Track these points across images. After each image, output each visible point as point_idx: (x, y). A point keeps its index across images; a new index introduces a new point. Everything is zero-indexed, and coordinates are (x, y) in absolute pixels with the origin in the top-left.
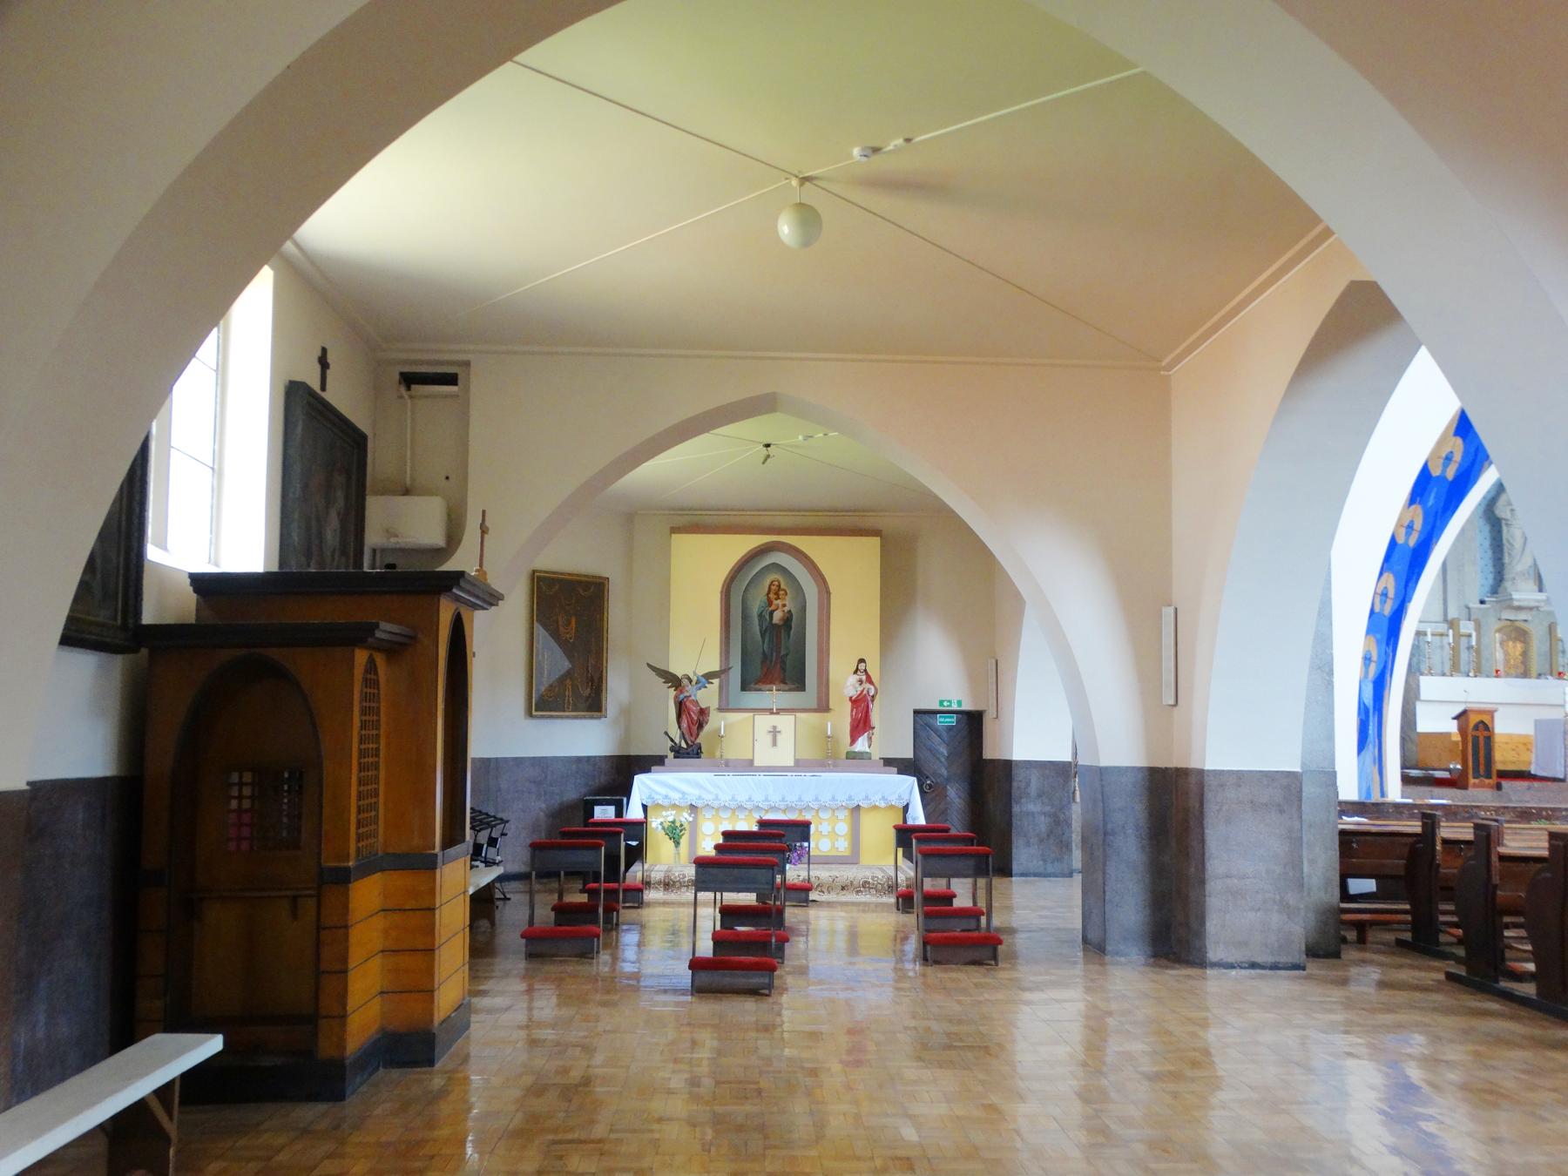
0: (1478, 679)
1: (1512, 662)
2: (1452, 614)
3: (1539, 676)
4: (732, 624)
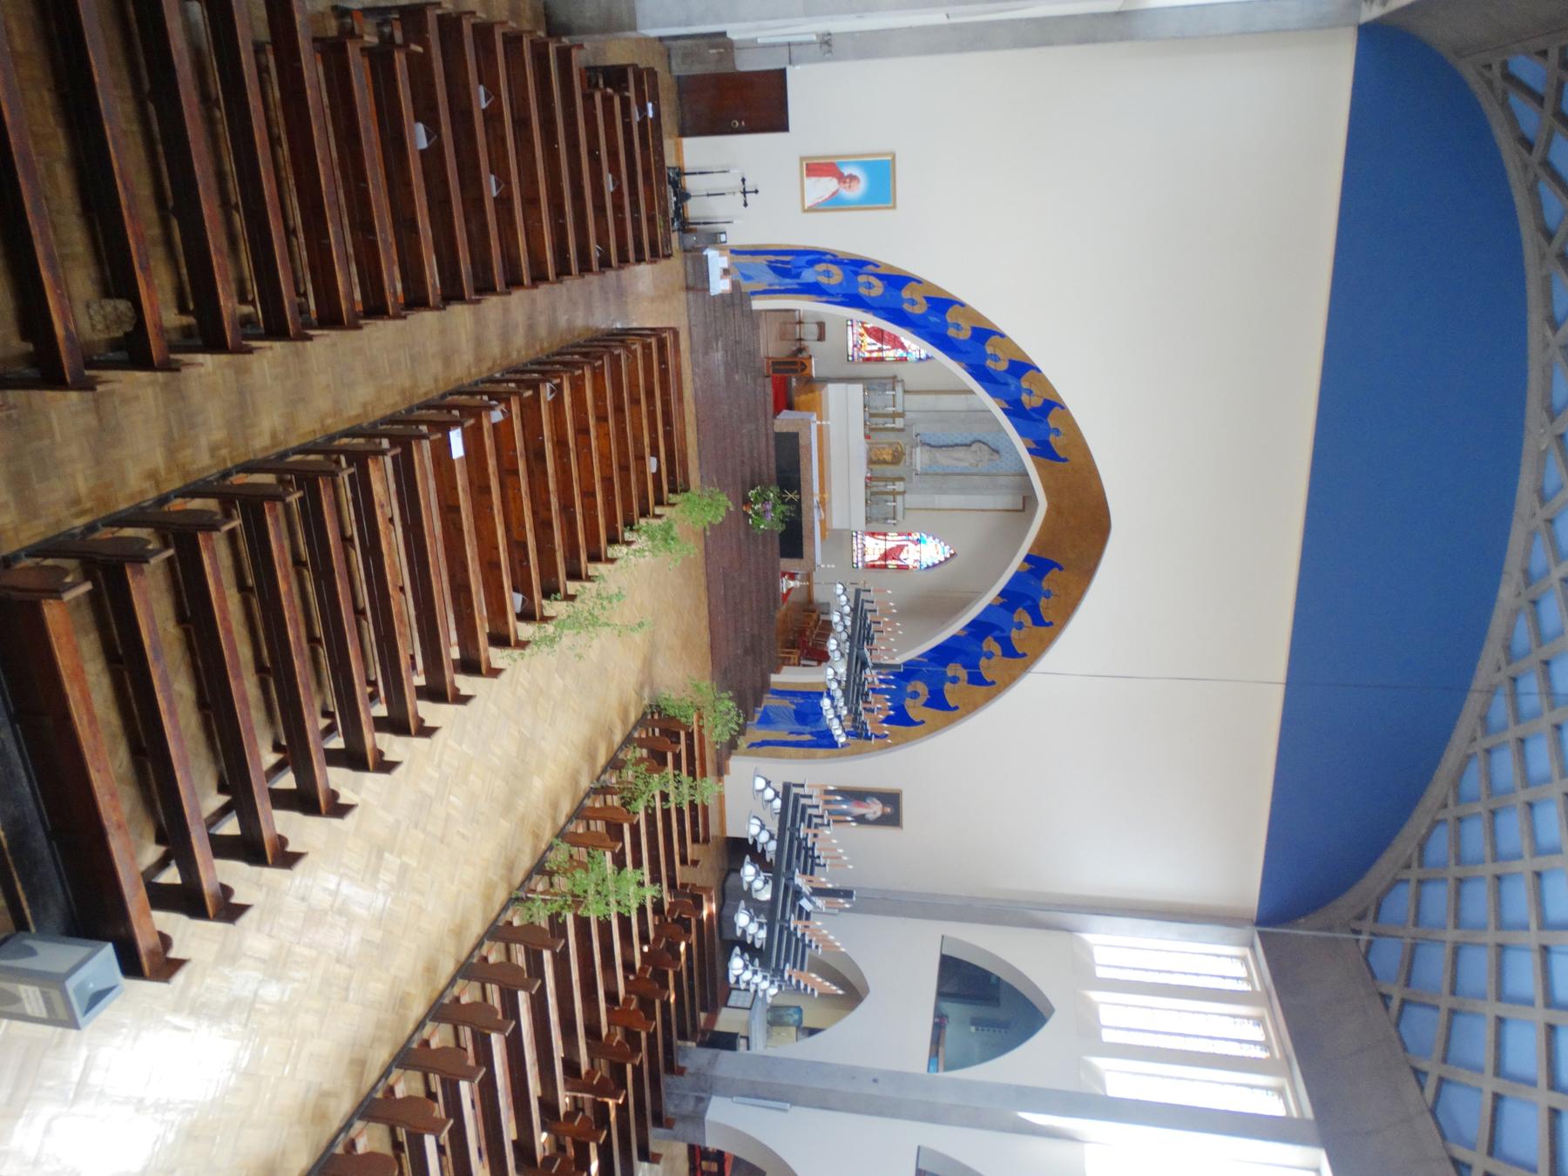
2: (909, 416)
4: (212, 181)
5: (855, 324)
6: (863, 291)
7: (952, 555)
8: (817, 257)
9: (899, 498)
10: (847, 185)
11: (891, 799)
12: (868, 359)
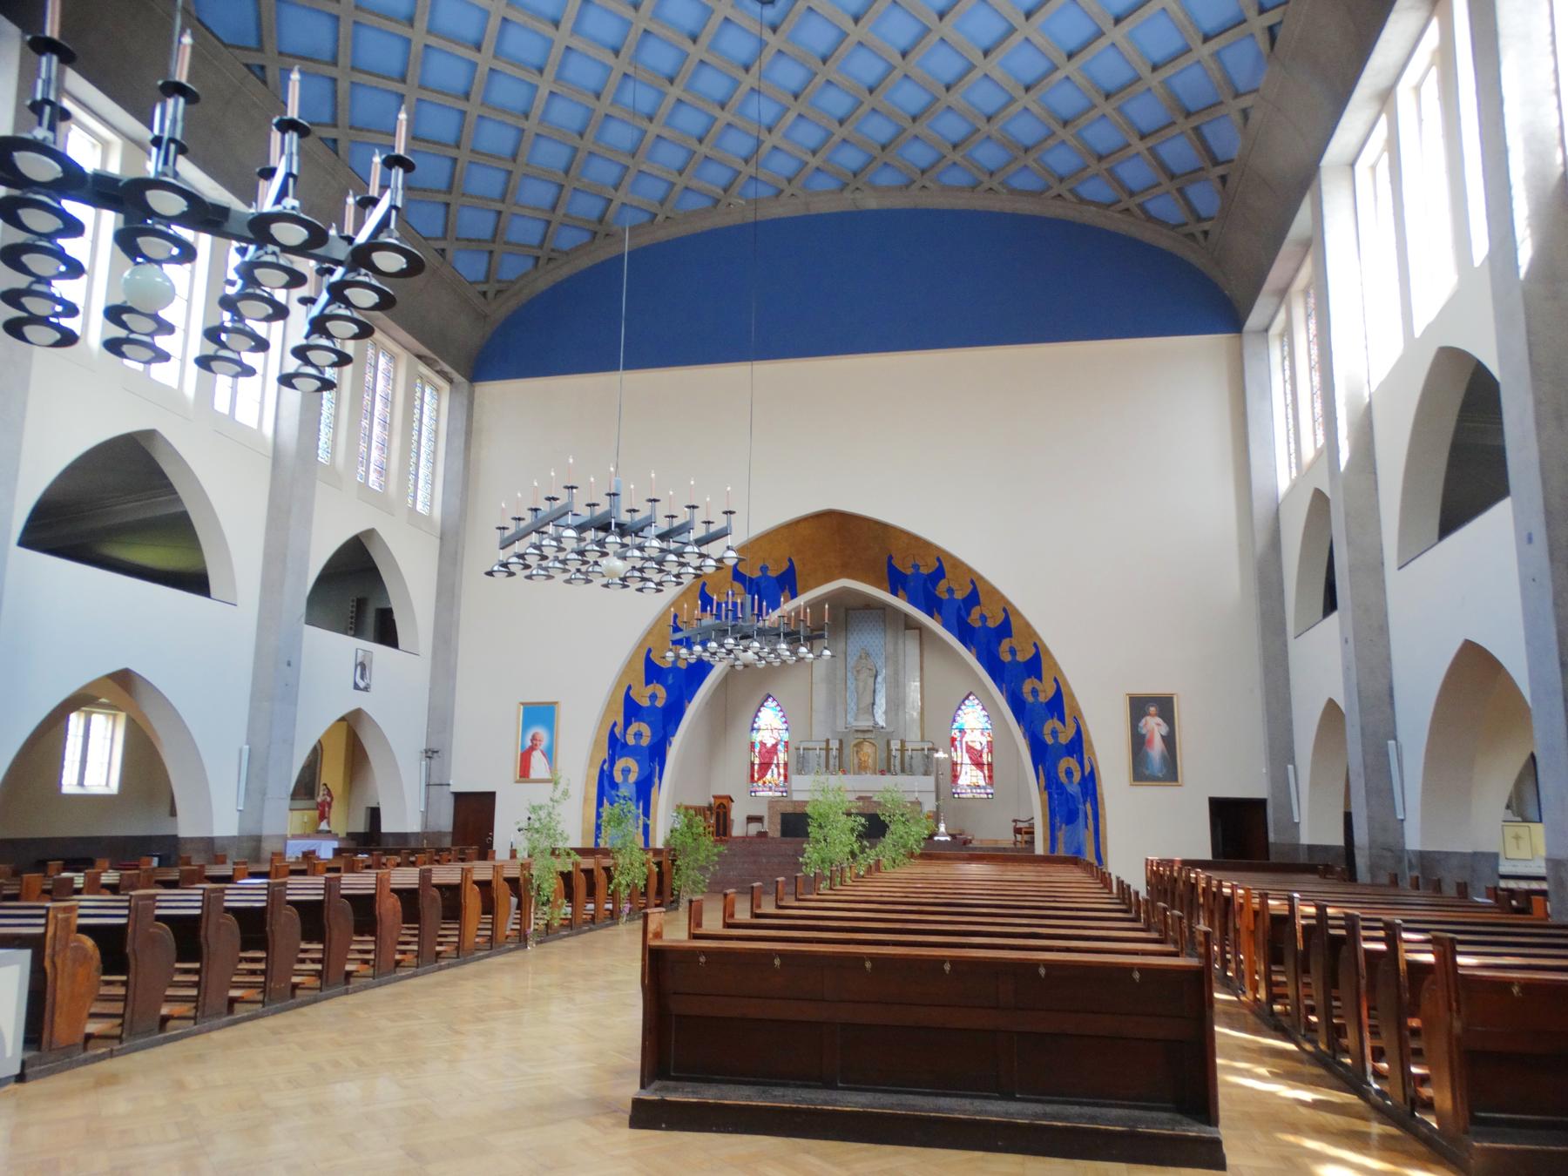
5: (753, 789)
8: (606, 783)
10: (538, 743)
11: (1139, 706)
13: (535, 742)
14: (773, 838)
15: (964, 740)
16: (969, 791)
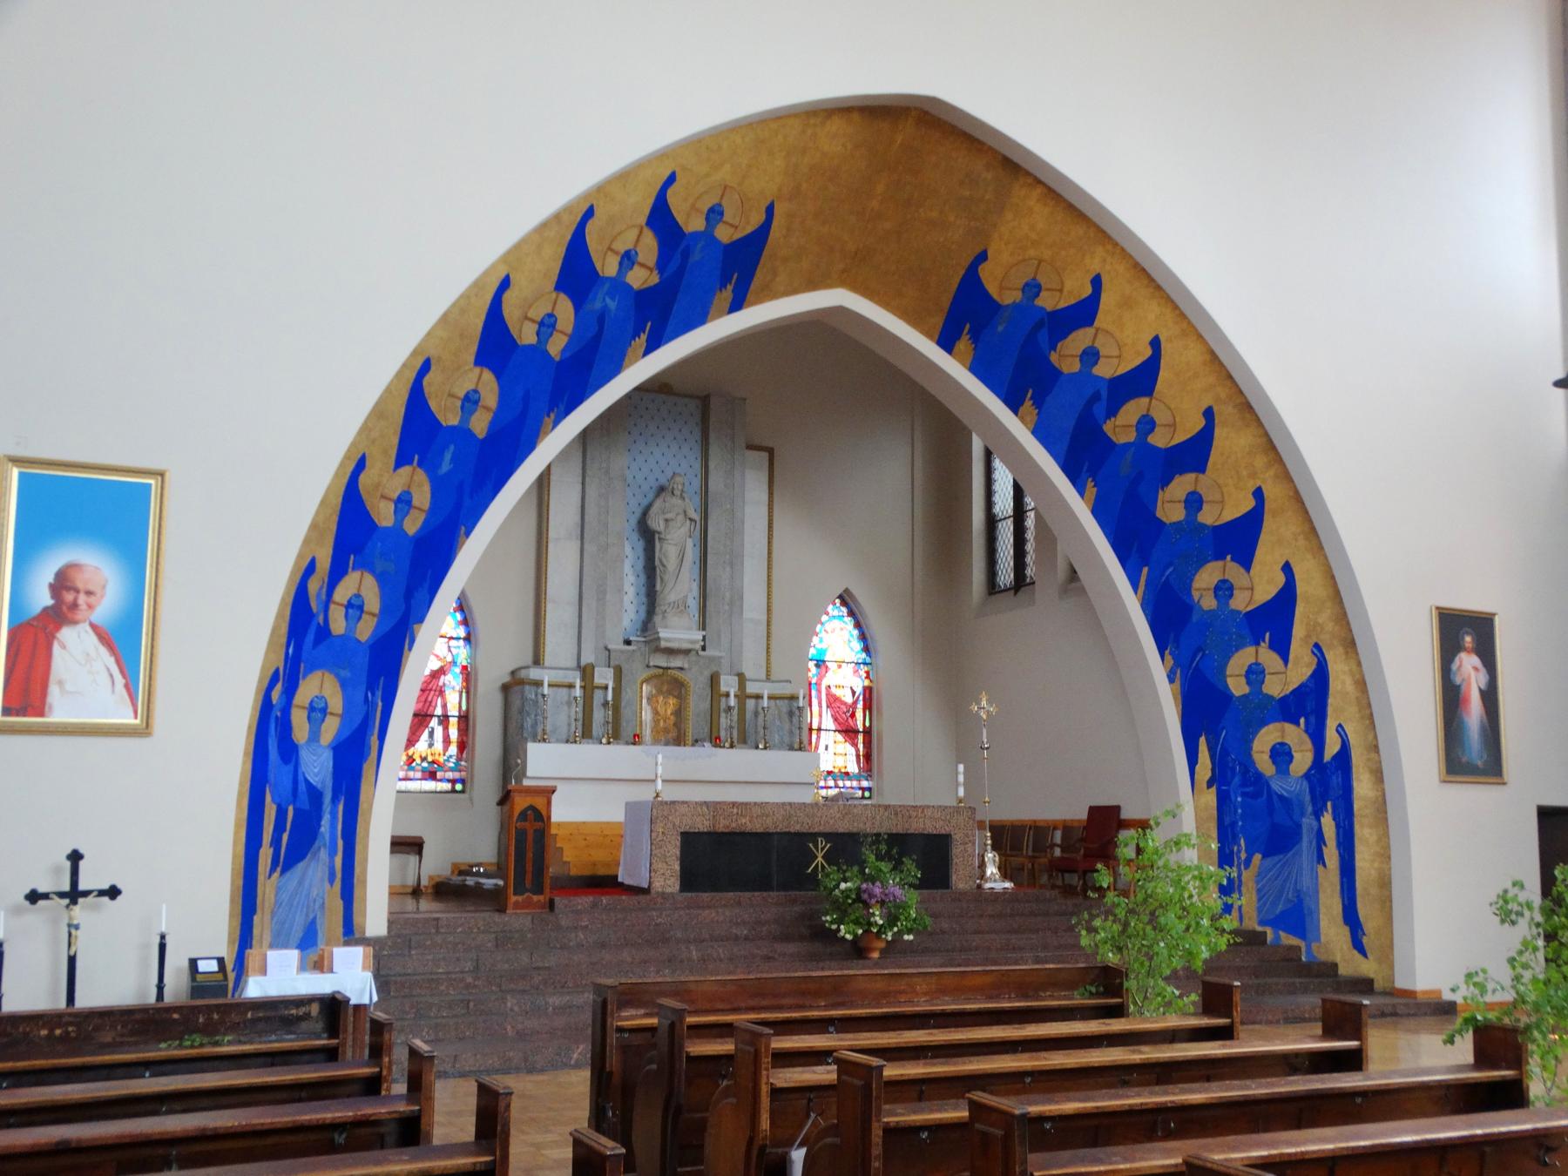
0: (611, 747)
1: (662, 723)
3: (696, 742)
6: (366, 630)
7: (844, 603)
9: (751, 688)
10: (82, 599)
12: (462, 746)
13: (69, 597)
14: (663, 895)
15: (825, 683)
16: (831, 783)
